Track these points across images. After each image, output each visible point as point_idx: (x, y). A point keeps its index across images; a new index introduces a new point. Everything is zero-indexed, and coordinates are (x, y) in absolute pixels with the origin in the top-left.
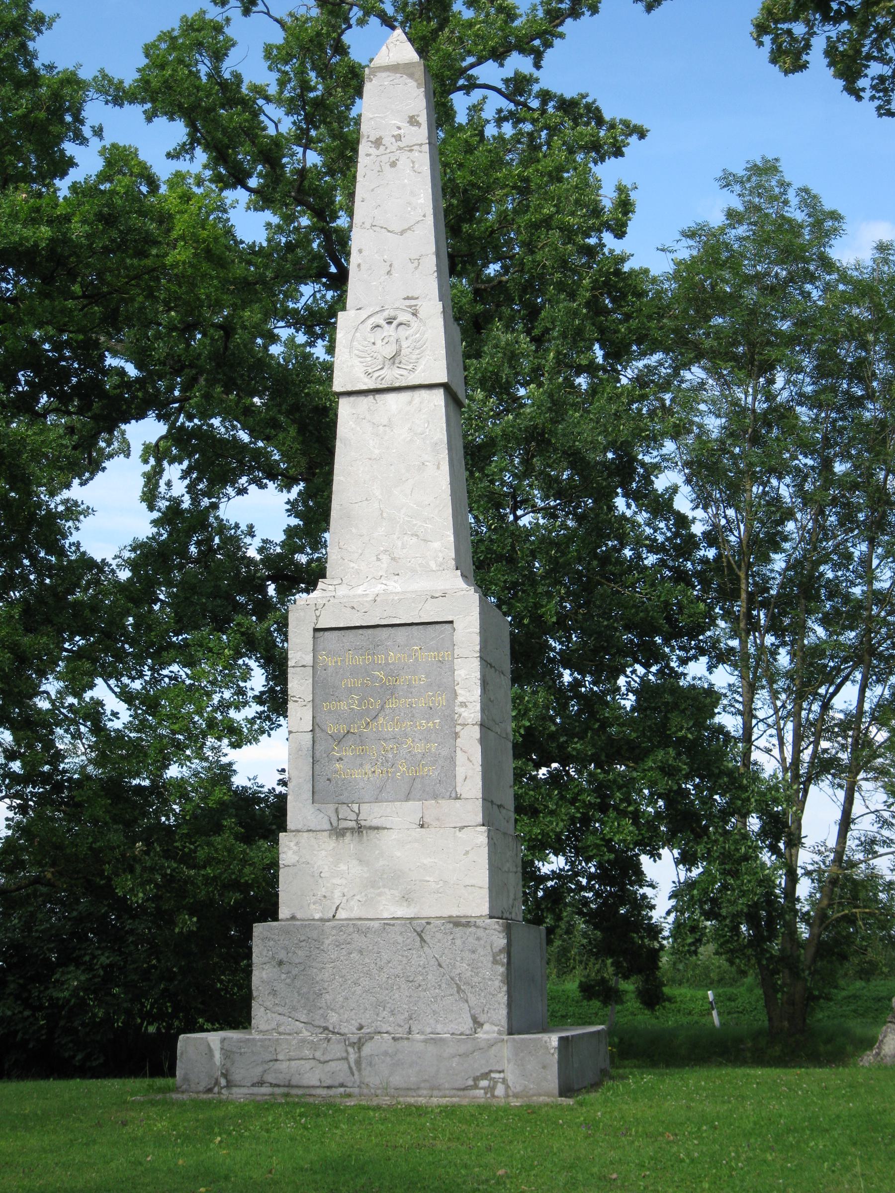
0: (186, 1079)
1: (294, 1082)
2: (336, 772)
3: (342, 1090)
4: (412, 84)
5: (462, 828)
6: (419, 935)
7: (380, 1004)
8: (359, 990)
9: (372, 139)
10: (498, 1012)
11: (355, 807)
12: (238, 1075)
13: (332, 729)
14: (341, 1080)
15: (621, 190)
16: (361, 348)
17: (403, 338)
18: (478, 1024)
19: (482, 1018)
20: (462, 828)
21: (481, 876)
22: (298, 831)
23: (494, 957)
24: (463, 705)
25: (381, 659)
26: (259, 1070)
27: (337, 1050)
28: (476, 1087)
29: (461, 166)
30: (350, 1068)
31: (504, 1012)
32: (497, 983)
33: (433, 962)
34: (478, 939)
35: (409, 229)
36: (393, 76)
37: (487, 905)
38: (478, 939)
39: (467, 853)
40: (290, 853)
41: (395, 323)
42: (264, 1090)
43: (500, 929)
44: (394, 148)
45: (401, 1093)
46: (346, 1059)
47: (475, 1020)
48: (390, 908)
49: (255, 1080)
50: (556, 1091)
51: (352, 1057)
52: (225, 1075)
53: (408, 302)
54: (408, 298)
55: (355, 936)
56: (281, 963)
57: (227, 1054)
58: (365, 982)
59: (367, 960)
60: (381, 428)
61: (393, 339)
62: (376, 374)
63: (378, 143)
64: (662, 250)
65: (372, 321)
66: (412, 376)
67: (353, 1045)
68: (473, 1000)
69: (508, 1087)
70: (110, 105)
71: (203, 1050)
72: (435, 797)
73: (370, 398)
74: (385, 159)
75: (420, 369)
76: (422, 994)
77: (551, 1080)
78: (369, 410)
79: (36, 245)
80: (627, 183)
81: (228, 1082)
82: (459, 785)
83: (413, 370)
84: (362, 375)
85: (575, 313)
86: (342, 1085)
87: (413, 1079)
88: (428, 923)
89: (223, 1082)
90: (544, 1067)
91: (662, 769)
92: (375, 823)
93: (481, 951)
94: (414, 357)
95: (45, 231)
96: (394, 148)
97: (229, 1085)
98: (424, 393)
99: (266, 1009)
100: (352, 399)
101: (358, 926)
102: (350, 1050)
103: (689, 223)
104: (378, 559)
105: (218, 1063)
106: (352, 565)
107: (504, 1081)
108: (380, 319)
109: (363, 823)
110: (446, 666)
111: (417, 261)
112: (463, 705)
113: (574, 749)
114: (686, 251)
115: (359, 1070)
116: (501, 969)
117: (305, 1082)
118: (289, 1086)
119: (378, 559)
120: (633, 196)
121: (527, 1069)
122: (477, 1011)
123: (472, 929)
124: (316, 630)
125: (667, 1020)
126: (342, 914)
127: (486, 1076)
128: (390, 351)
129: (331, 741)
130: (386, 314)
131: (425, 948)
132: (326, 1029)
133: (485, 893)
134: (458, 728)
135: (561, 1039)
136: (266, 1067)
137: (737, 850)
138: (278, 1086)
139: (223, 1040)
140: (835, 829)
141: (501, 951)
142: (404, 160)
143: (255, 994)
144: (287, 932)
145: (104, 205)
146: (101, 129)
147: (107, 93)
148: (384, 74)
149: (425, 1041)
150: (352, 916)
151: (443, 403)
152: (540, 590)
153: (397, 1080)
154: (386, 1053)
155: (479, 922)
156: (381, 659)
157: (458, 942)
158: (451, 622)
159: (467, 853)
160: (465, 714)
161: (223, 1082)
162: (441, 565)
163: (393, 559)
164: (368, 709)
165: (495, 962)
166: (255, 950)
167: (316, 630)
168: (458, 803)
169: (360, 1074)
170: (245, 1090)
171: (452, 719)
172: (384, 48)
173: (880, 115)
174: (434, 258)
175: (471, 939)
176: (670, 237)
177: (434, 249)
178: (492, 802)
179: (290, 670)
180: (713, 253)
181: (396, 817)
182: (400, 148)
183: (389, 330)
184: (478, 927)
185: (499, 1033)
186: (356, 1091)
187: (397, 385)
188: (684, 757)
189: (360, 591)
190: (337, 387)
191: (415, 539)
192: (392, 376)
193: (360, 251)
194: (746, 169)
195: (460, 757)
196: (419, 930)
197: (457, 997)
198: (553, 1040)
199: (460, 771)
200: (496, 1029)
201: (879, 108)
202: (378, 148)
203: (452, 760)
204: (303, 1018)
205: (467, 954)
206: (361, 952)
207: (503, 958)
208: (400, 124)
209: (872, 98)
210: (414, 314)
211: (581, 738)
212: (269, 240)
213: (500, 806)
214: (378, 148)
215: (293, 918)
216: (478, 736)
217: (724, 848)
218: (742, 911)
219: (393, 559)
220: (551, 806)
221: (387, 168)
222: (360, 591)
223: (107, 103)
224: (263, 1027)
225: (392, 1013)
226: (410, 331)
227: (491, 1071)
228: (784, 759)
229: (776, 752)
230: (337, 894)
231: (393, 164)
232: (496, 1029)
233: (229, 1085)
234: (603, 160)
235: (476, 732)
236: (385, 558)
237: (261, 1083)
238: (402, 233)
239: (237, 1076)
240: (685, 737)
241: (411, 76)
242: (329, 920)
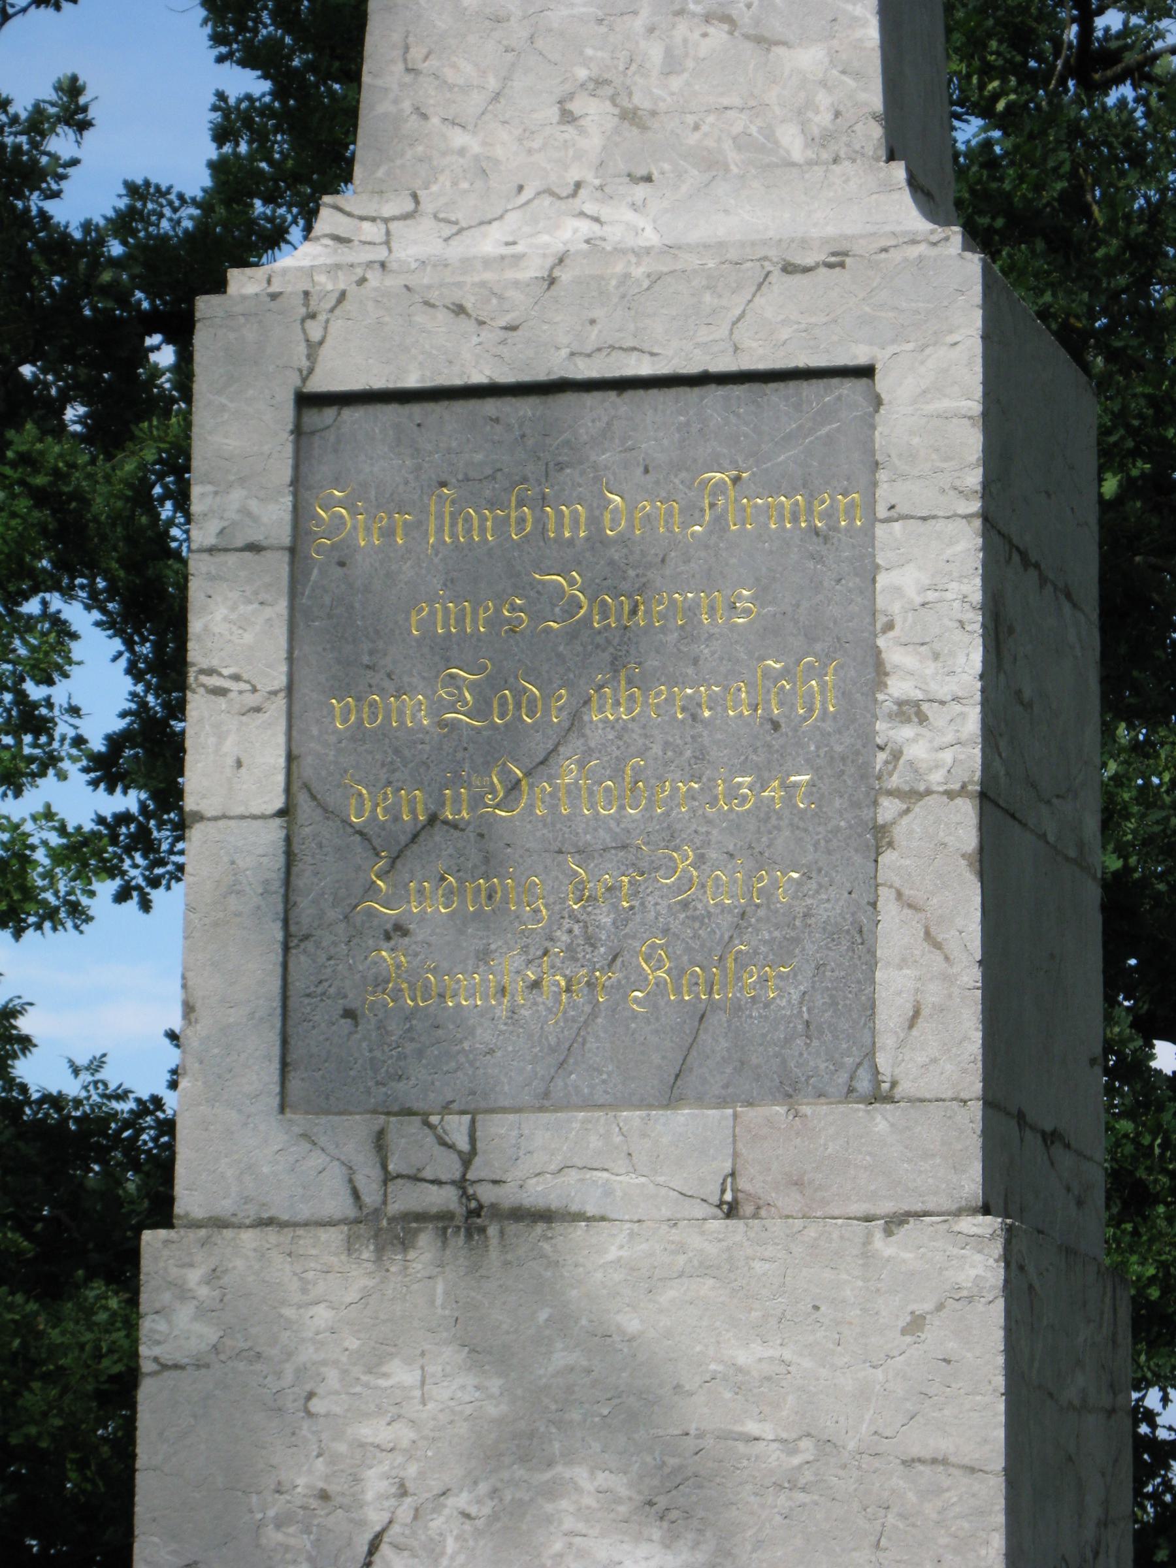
2: (380, 982)
11: (457, 1128)
24: (911, 711)
39: (916, 1324)
40: (184, 1315)
72: (789, 1091)
82: (887, 1041)
92: (538, 1191)
104: (568, 117)
106: (459, 138)
109: (486, 1194)
112: (911, 711)
119: (568, 117)
134: (888, 809)
158: (866, 372)
159: (916, 1324)
162: (826, 138)
163: (630, 116)
167: (307, 401)
168: (881, 1120)
171: (865, 773)
189: (489, 242)
191: (718, 34)
195: (895, 930)
199: (895, 986)
203: (860, 937)
219: (630, 116)
222: (489, 242)
235: (961, 826)
236: (595, 112)
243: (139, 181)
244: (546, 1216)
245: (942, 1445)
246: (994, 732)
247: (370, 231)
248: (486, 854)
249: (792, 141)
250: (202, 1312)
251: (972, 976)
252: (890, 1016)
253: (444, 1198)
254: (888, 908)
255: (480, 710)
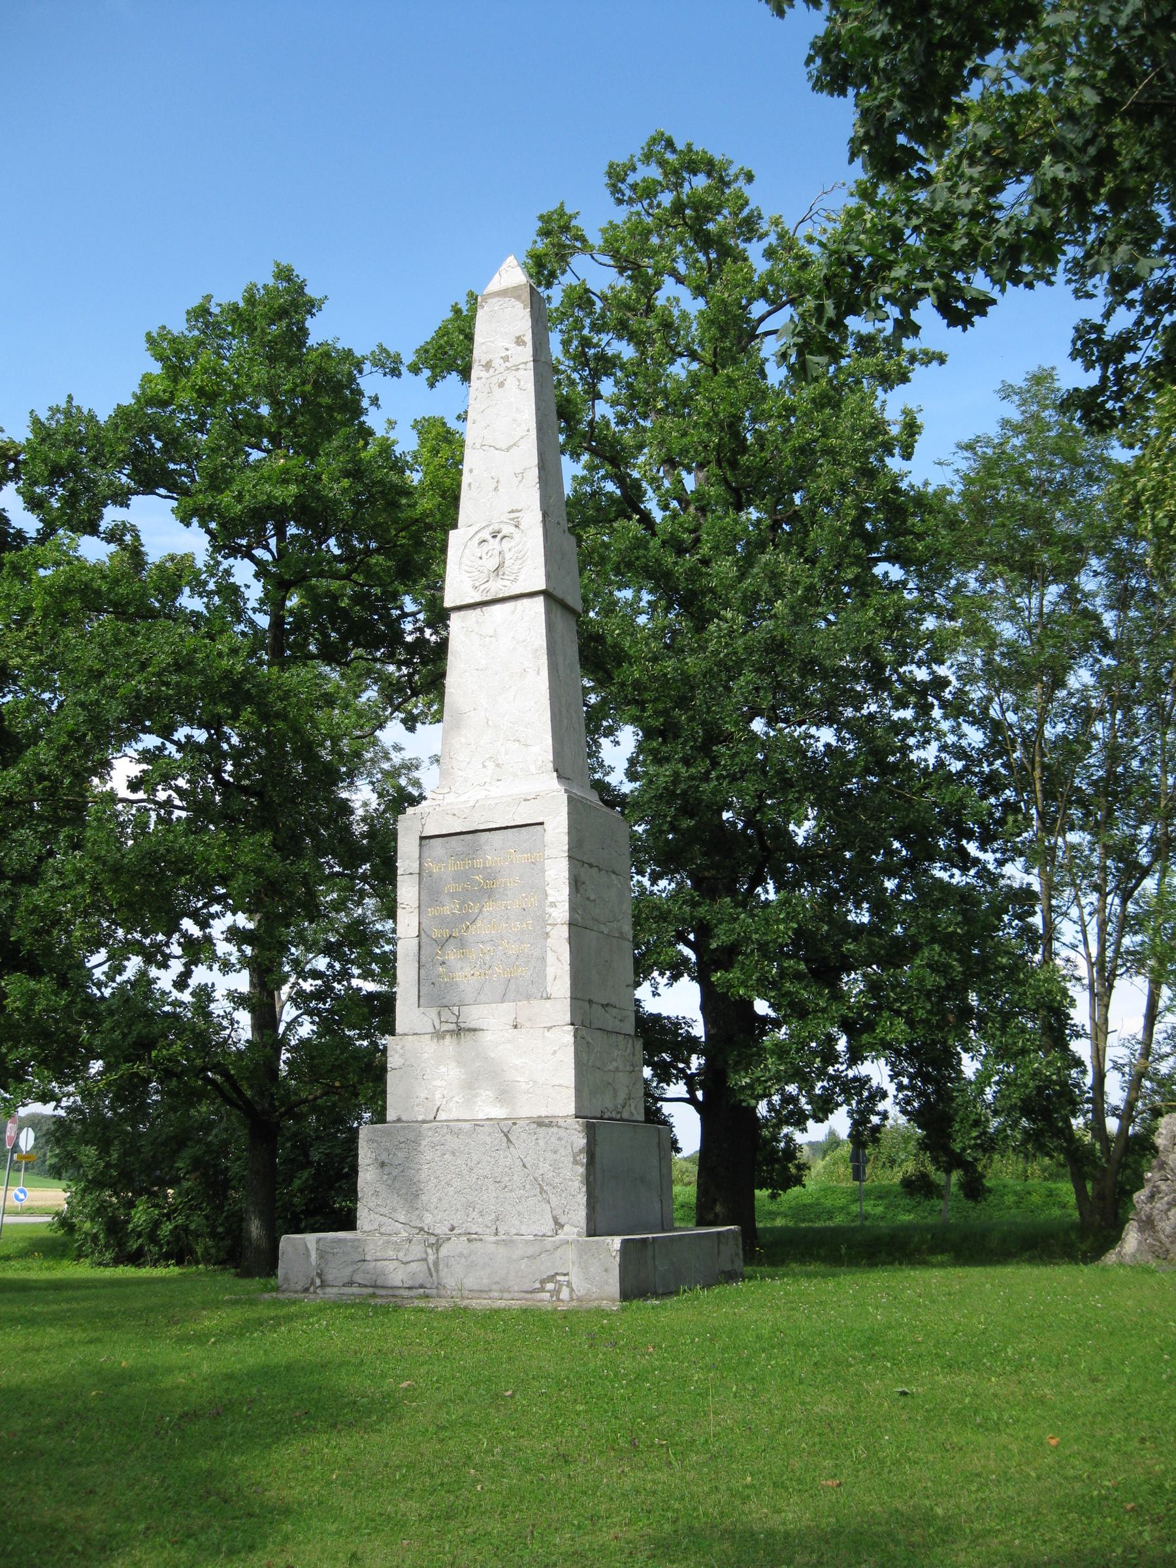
0: (286, 1279)
1: (379, 1283)
4: (519, 305)
5: (549, 1028)
7: (471, 1205)
10: (578, 1214)
11: (455, 1010)
12: (331, 1275)
13: (436, 934)
15: (906, 412)
18: (559, 1225)
19: (562, 1220)
20: (549, 1028)
21: (567, 1075)
24: (553, 905)
25: (479, 863)
26: (349, 1270)
28: (542, 1290)
31: (583, 1213)
32: (577, 1184)
33: (518, 1163)
34: (560, 1139)
36: (502, 300)
38: (560, 1139)
39: (555, 1052)
42: (355, 1290)
44: (501, 369)
46: (425, 1260)
47: (556, 1222)
48: (488, 1108)
50: (617, 1295)
51: (431, 1258)
52: (320, 1275)
55: (449, 1137)
56: (383, 1164)
57: (322, 1254)
58: (457, 1183)
61: (496, 552)
63: (488, 366)
68: (554, 1200)
71: (302, 1249)
72: (528, 997)
73: (478, 611)
75: (521, 577)
76: (508, 1195)
77: (612, 1285)
79: (284, 503)
84: (471, 590)
86: (421, 1287)
87: (485, 1281)
89: (318, 1282)
92: (472, 1025)
93: (562, 1151)
95: (293, 489)
96: (501, 369)
97: (324, 1285)
98: (525, 602)
101: (452, 1128)
102: (429, 1250)
107: (569, 1284)
108: (485, 534)
110: (537, 865)
112: (553, 905)
114: (964, 463)
115: (437, 1271)
116: (581, 1170)
117: (390, 1283)
118: (375, 1286)
120: (920, 419)
121: (591, 1271)
122: (558, 1212)
123: (555, 1129)
124: (422, 838)
125: (979, 1214)
126: (442, 1116)
127: (551, 1278)
128: (493, 563)
130: (491, 529)
132: (421, 1229)
133: (571, 1092)
134: (549, 928)
135: (624, 1242)
139: (319, 1240)
140: (1141, 1022)
141: (581, 1151)
142: (511, 382)
144: (389, 1134)
147: (383, 366)
148: (494, 300)
151: (542, 610)
153: (470, 1282)
154: (461, 1255)
155: (561, 1122)
156: (479, 863)
157: (541, 1142)
159: (555, 1052)
161: (318, 1282)
163: (498, 765)
165: (575, 1162)
166: (361, 1151)
167: (422, 838)
168: (548, 1003)
170: (335, 1290)
171: (544, 920)
173: (1078, 298)
175: (553, 1140)
176: (946, 451)
178: (590, 1002)
180: (993, 466)
181: (491, 1018)
183: (494, 544)
185: (579, 1235)
186: (434, 1292)
189: (464, 798)
190: (447, 604)
192: (498, 588)
195: (550, 957)
198: (616, 1242)
199: (550, 971)
201: (1076, 291)
204: (402, 1219)
205: (549, 1155)
206: (453, 1153)
207: (583, 1158)
209: (1069, 281)
211: (855, 939)
215: (399, 1120)
219: (498, 765)
220: (822, 1004)
221: (496, 389)
222: (464, 798)
224: (367, 1227)
225: (481, 1214)
226: (513, 543)
228: (1089, 955)
229: (1081, 948)
230: (438, 1096)
231: (501, 385)
233: (324, 1285)
234: (892, 388)
235: (564, 931)
236: (490, 764)
237: (350, 1283)
238: (508, 449)
241: (518, 298)
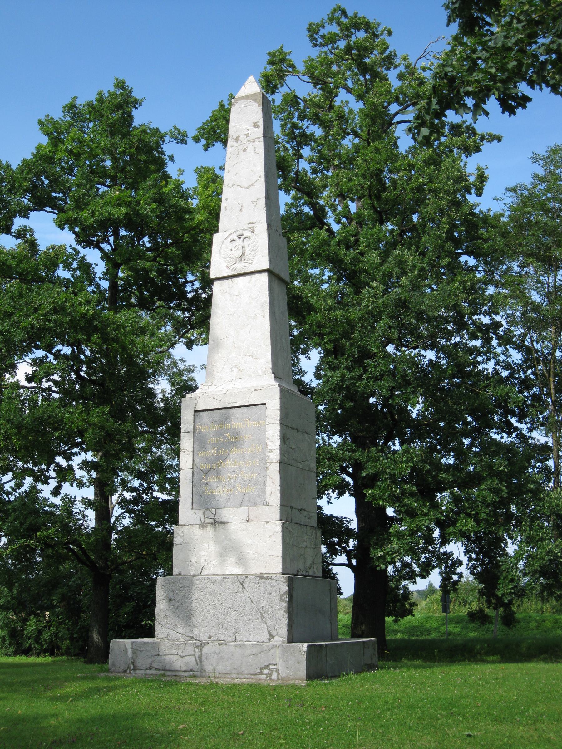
0: (113, 665)
1: (167, 668)
2: (204, 491)
3: (192, 673)
4: (256, 105)
6: (242, 584)
7: (220, 624)
8: (209, 615)
9: (235, 137)
10: (283, 630)
11: (213, 511)
13: (203, 467)
14: (191, 668)
15: (479, 169)
16: (225, 253)
17: (246, 246)
18: (271, 636)
19: (274, 633)
21: (277, 550)
22: (184, 525)
23: (281, 597)
24: (271, 451)
26: (150, 660)
27: (189, 650)
28: (261, 673)
29: (372, 160)
30: (196, 660)
32: (282, 612)
33: (248, 600)
34: (273, 586)
35: (252, 185)
37: (281, 567)
38: (273, 586)
39: (270, 536)
40: (179, 537)
41: (243, 237)
43: (285, 581)
44: (245, 141)
45: (223, 676)
46: (194, 655)
49: (148, 666)
50: (305, 677)
52: (133, 663)
53: (250, 226)
54: (250, 223)
55: (208, 584)
57: (134, 651)
58: (213, 611)
59: (214, 599)
60: (235, 297)
62: (232, 267)
63: (237, 139)
64: (496, 199)
65: (231, 237)
66: (251, 266)
67: (197, 647)
69: (279, 674)
70: (180, 144)
71: (123, 647)
72: (255, 504)
74: (241, 148)
75: (254, 262)
77: (302, 671)
78: (229, 287)
79: (118, 217)
80: (482, 165)
81: (134, 667)
82: (268, 497)
83: (251, 263)
84: (225, 268)
85: (439, 237)
86: (191, 670)
87: (228, 668)
88: (246, 577)
89: (132, 667)
90: (298, 663)
91: (490, 490)
92: (224, 520)
94: (252, 256)
95: (124, 210)
97: (135, 669)
98: (257, 276)
99: (162, 626)
100: (220, 282)
102: (196, 650)
103: (512, 184)
104: (232, 371)
105: (130, 656)
106: (218, 374)
107: (277, 670)
109: (217, 520)
110: (262, 429)
111: (255, 203)
112: (271, 451)
113: (442, 477)
116: (285, 604)
118: (165, 670)
119: (232, 371)
120: (487, 173)
121: (289, 663)
122: (271, 629)
123: (270, 581)
124: (195, 412)
127: (267, 667)
128: (238, 253)
129: (202, 474)
130: (237, 233)
131: (245, 592)
132: (192, 637)
134: (268, 464)
136: (154, 659)
137: (537, 535)
138: (159, 670)
141: (285, 594)
143: (157, 617)
145: (156, 194)
146: (173, 157)
147: (176, 138)
148: (241, 101)
149: (235, 646)
150: (210, 573)
152: (409, 391)
154: (215, 653)
155: (274, 577)
157: (262, 588)
158: (265, 404)
159: (270, 536)
160: (271, 457)
161: (132, 667)
162: (264, 371)
163: (240, 370)
164: (221, 455)
165: (282, 600)
167: (195, 412)
168: (267, 508)
169: (201, 664)
170: (142, 672)
171: (265, 460)
172: (243, 87)
174: (264, 200)
175: (269, 587)
177: (264, 195)
179: (182, 434)
182: (249, 141)
183: (239, 242)
184: (273, 580)
185: (283, 642)
187: (243, 272)
188: (504, 483)
189: (220, 388)
191: (251, 358)
192: (242, 267)
193: (227, 200)
194: (547, 151)
195: (269, 482)
196: (241, 581)
197: (260, 620)
199: (269, 489)
200: (281, 639)
202: (237, 142)
203: (264, 482)
205: (266, 596)
206: (211, 594)
207: (286, 598)
208: (249, 128)
210: (252, 232)
212: (287, 212)
213: (300, 510)
214: (237, 142)
216: (278, 469)
217: (530, 534)
218: (537, 569)
219: (240, 370)
221: (241, 152)
222: (220, 388)
223: (178, 143)
226: (250, 241)
227: (270, 664)
230: (203, 560)
231: (245, 150)
232: (281, 639)
234: (470, 155)
235: (277, 467)
236: (235, 369)
237: (150, 668)
238: (248, 188)
239: (139, 664)
240: (503, 471)
241: (255, 100)
242: (198, 575)
243: (528, 104)
244: (224, 523)
245: (274, 553)
246: (282, 454)
247: (206, 388)
248: (218, 474)
249: (260, 372)
250: (182, 537)
251: (279, 488)
252: (268, 493)
253: (212, 521)
254: (268, 478)
255: (217, 453)
